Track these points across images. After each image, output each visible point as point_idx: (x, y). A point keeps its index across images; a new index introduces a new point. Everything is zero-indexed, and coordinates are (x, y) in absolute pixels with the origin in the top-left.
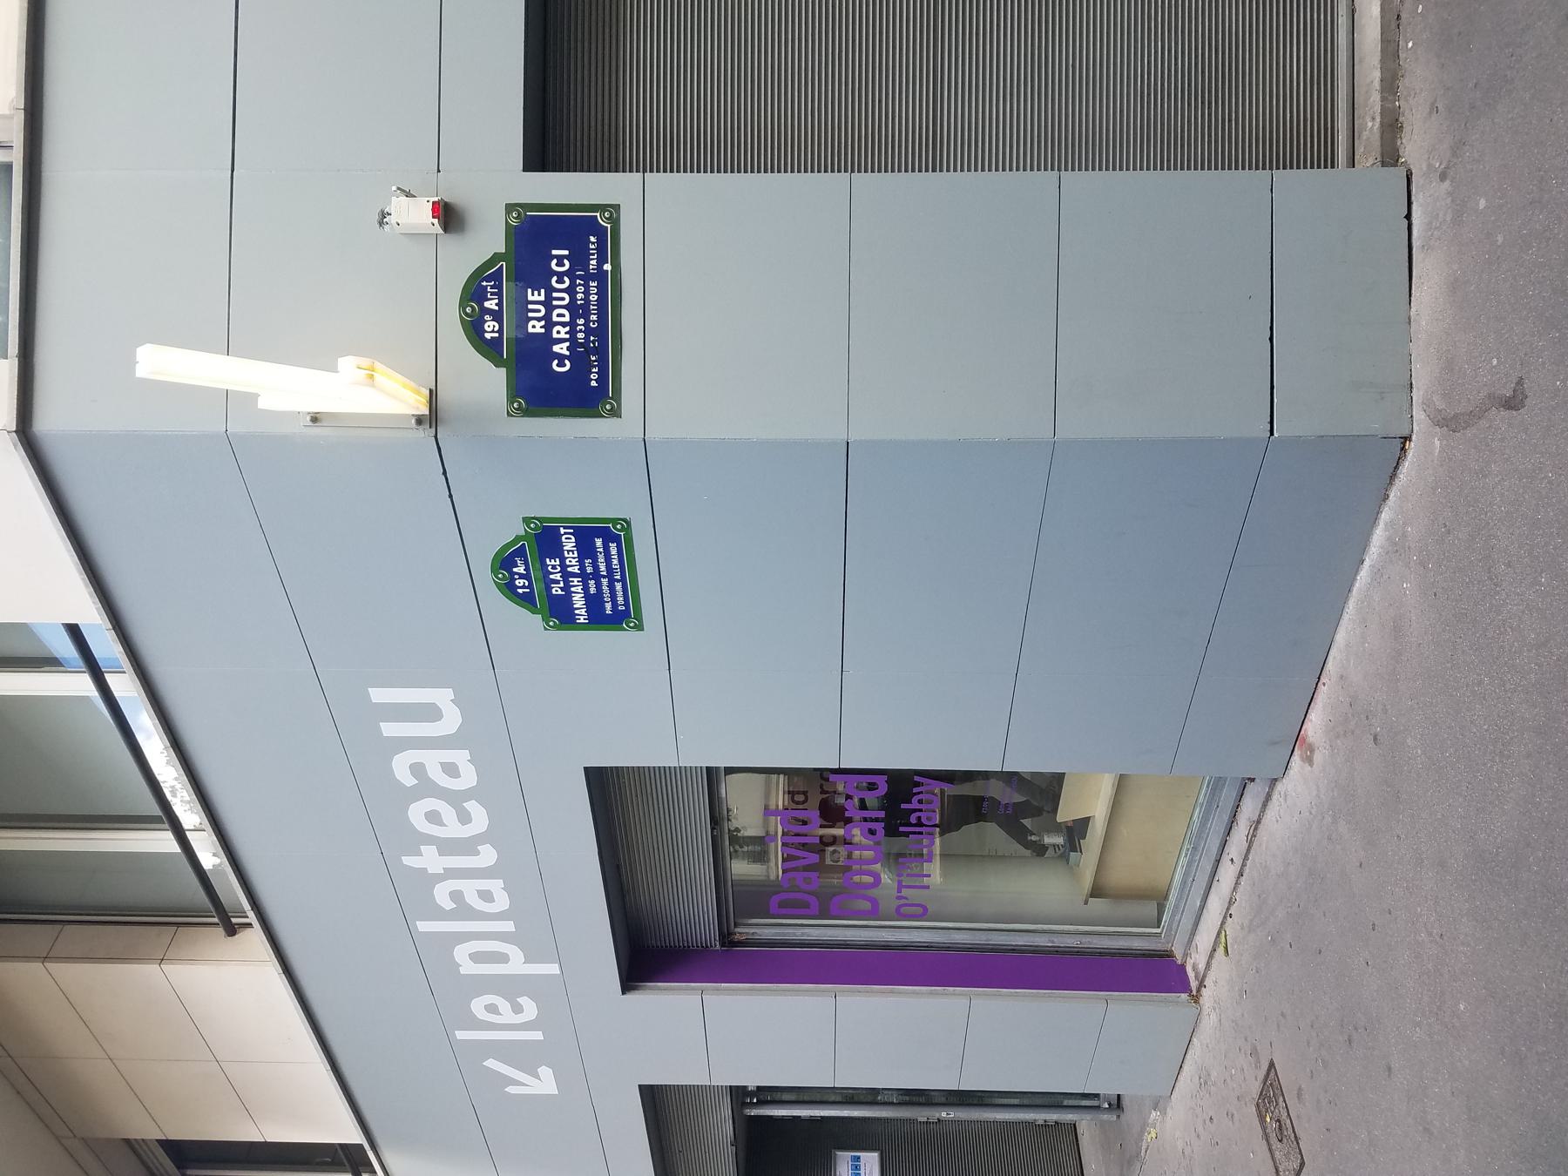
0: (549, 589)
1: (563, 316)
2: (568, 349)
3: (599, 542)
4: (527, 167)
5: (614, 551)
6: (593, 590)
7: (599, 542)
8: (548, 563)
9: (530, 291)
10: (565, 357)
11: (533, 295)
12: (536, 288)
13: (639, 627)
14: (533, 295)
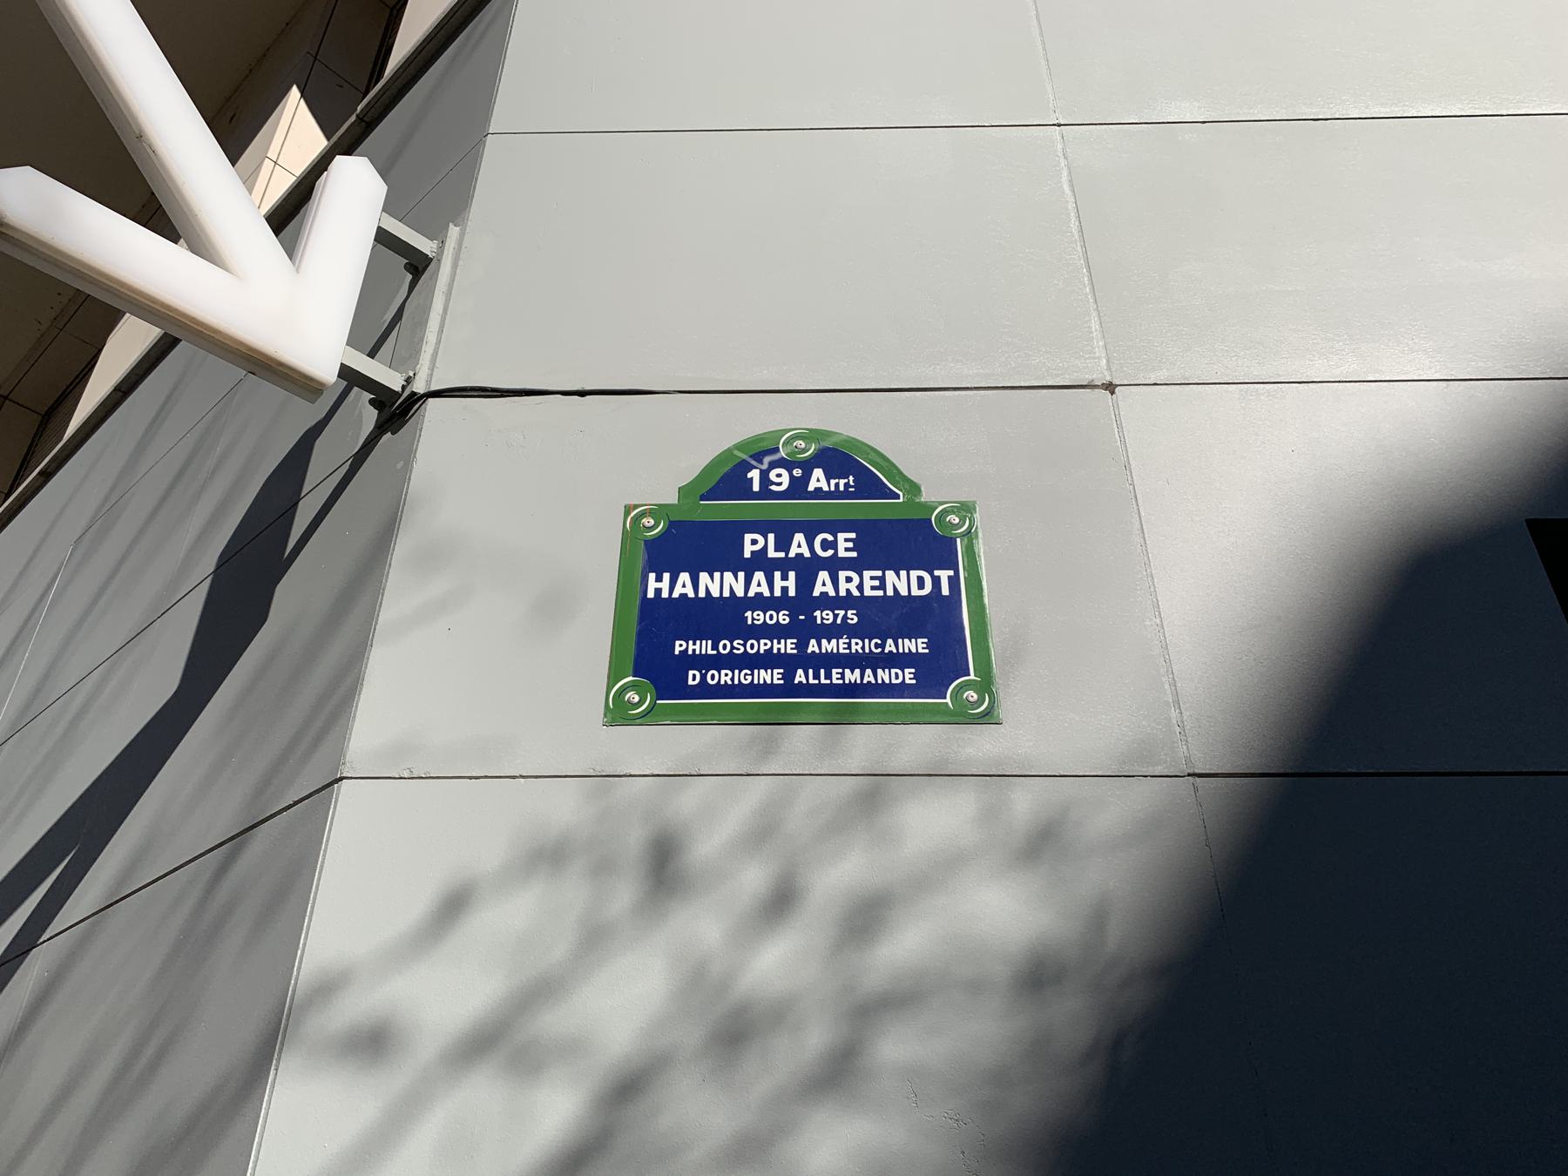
0: (762, 528)
1: (694, 679)
2: (800, 682)
3: (917, 646)
4: (788, 587)
5: (763, 676)
6: (756, 617)
7: (917, 646)
8: (841, 536)
9: (853, 535)
10: (883, 649)
11: (846, 540)
12: (857, 545)
13: (618, 714)
14: (846, 540)
